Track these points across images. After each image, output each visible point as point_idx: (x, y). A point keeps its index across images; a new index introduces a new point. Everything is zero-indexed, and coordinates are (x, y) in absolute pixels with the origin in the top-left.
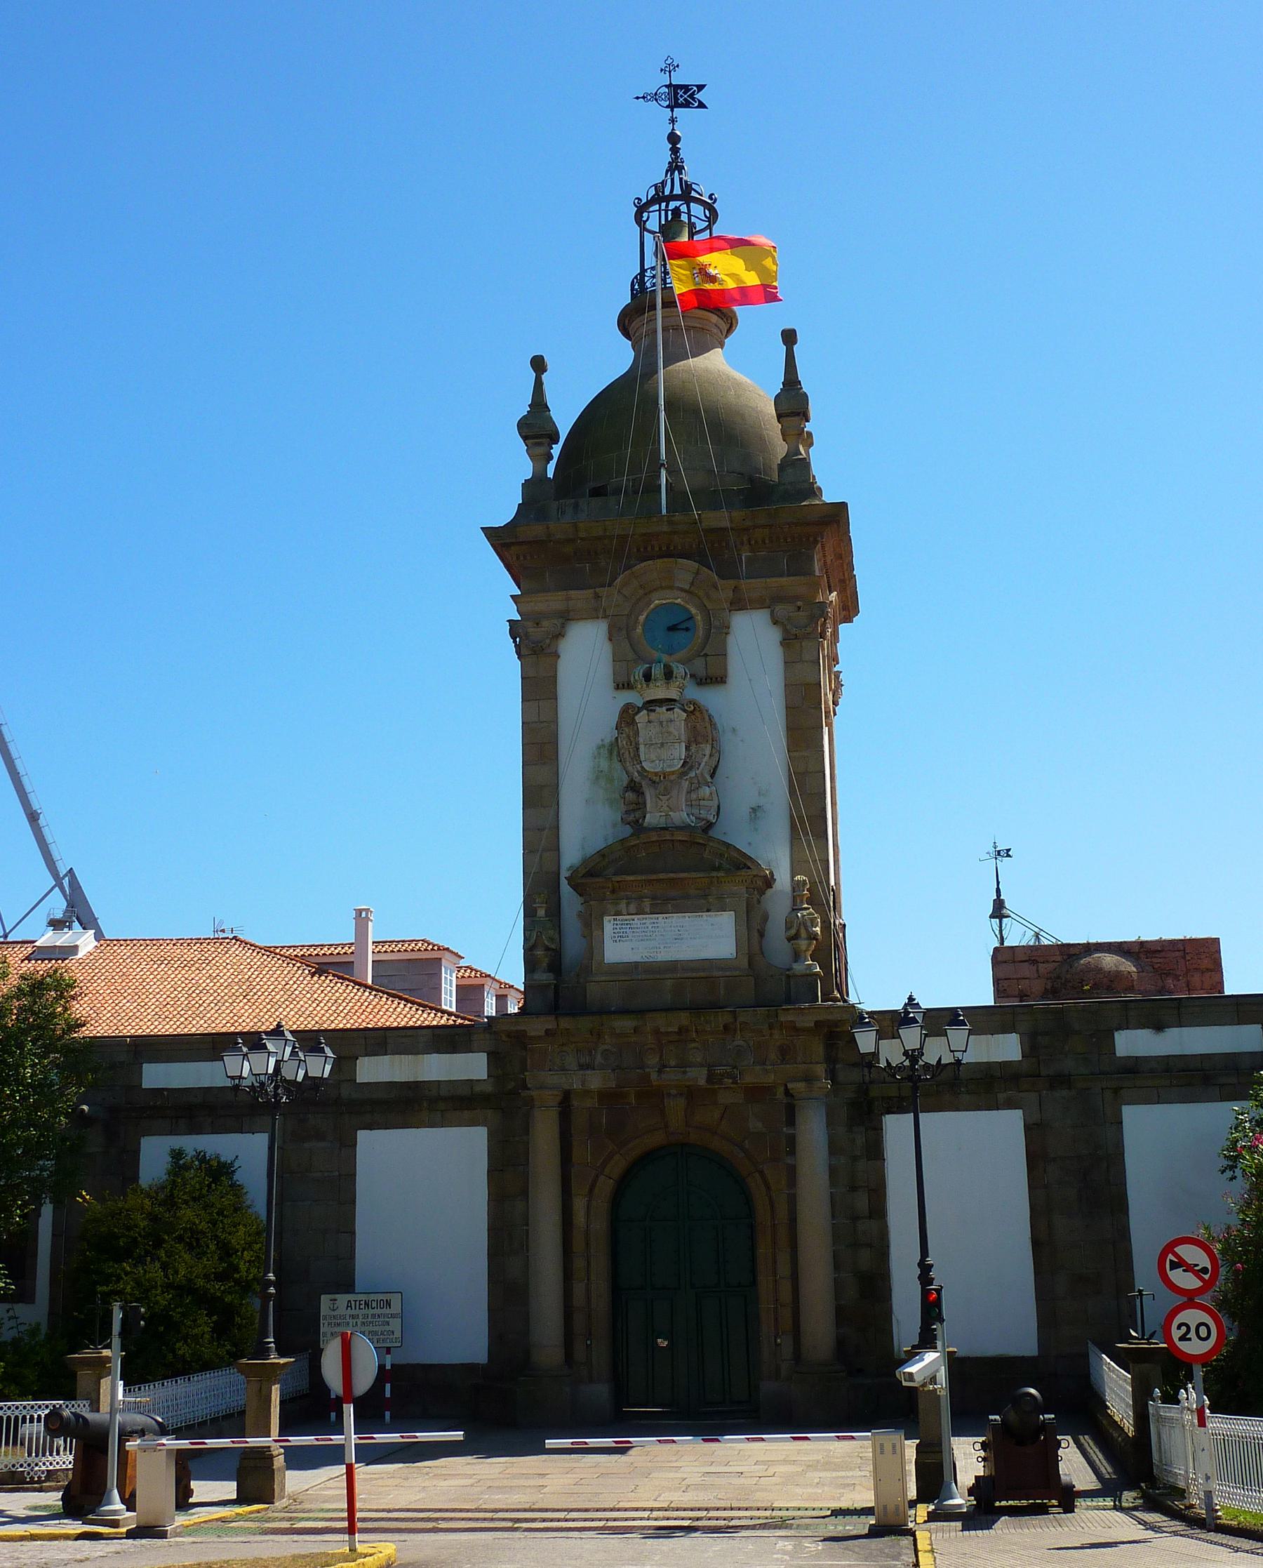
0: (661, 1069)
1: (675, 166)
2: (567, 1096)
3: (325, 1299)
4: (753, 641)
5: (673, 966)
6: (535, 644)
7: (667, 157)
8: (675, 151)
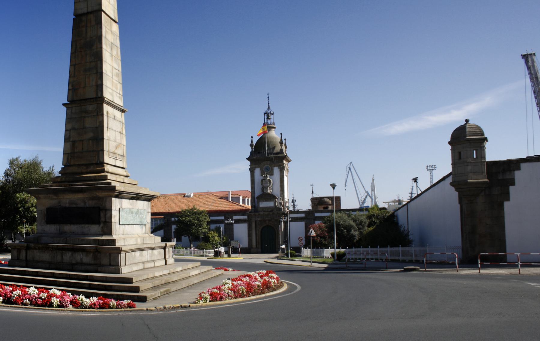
1: (269, 107)
4: (276, 170)
5: (267, 207)
6: (252, 171)
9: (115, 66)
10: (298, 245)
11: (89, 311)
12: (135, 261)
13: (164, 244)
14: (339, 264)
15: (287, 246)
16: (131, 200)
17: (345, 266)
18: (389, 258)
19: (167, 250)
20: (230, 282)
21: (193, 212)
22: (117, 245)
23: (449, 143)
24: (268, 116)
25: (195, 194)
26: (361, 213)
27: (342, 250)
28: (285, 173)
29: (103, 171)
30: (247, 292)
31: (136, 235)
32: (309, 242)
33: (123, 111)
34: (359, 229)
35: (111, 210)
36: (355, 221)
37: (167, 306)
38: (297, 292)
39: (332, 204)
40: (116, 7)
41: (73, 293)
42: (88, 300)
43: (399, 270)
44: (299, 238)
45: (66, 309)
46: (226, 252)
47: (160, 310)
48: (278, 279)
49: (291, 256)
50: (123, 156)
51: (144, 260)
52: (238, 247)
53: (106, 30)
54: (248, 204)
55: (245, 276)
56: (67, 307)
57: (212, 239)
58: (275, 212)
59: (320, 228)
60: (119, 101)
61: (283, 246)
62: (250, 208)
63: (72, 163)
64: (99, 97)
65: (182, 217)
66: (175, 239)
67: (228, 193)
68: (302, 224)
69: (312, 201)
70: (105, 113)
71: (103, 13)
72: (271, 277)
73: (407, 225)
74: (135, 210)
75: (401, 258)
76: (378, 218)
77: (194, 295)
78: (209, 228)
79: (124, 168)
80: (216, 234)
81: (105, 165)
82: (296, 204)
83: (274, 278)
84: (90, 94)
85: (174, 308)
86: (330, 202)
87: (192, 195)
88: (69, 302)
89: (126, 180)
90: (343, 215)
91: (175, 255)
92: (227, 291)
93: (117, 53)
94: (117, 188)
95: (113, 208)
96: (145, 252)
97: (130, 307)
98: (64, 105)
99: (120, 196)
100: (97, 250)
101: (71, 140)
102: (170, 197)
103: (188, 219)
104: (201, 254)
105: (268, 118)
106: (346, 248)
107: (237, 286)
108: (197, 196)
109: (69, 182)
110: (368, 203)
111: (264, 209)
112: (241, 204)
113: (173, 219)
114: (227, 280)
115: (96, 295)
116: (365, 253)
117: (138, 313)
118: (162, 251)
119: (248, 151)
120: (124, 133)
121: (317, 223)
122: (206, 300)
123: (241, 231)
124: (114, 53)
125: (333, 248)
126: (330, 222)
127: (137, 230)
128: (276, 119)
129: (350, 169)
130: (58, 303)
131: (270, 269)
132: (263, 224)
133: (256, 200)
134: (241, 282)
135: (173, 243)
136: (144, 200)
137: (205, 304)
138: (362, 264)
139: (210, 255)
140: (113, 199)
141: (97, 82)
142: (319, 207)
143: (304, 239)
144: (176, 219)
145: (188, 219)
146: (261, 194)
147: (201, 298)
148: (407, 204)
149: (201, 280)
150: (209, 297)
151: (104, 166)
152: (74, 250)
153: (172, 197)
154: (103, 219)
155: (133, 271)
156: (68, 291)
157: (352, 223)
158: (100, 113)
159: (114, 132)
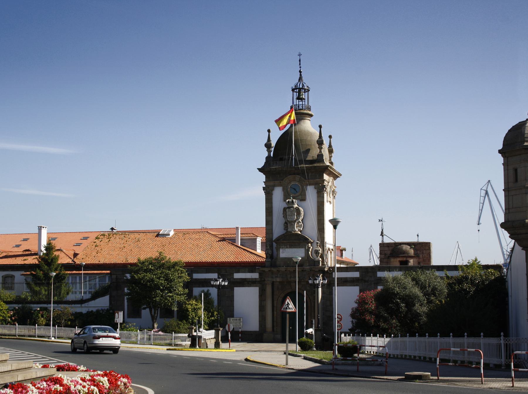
0: (291, 277)
1: (300, 79)
2: (273, 282)
3: (228, 319)
4: (311, 192)
6: (268, 191)
8: (301, 75)
21: (159, 265)
23: (500, 152)
24: (299, 92)
25: (177, 231)
36: (422, 287)
57: (192, 314)
65: (137, 272)
86: (412, 252)
87: (172, 233)
102: (132, 236)
103: (149, 276)
104: (168, 342)
105: (299, 98)
119: (261, 156)
123: (247, 301)
128: (314, 101)
129: (487, 193)
133: (275, 245)
139: (184, 343)
142: (392, 260)
145: (149, 276)
146: (283, 235)
153: (136, 235)
157: (417, 291)
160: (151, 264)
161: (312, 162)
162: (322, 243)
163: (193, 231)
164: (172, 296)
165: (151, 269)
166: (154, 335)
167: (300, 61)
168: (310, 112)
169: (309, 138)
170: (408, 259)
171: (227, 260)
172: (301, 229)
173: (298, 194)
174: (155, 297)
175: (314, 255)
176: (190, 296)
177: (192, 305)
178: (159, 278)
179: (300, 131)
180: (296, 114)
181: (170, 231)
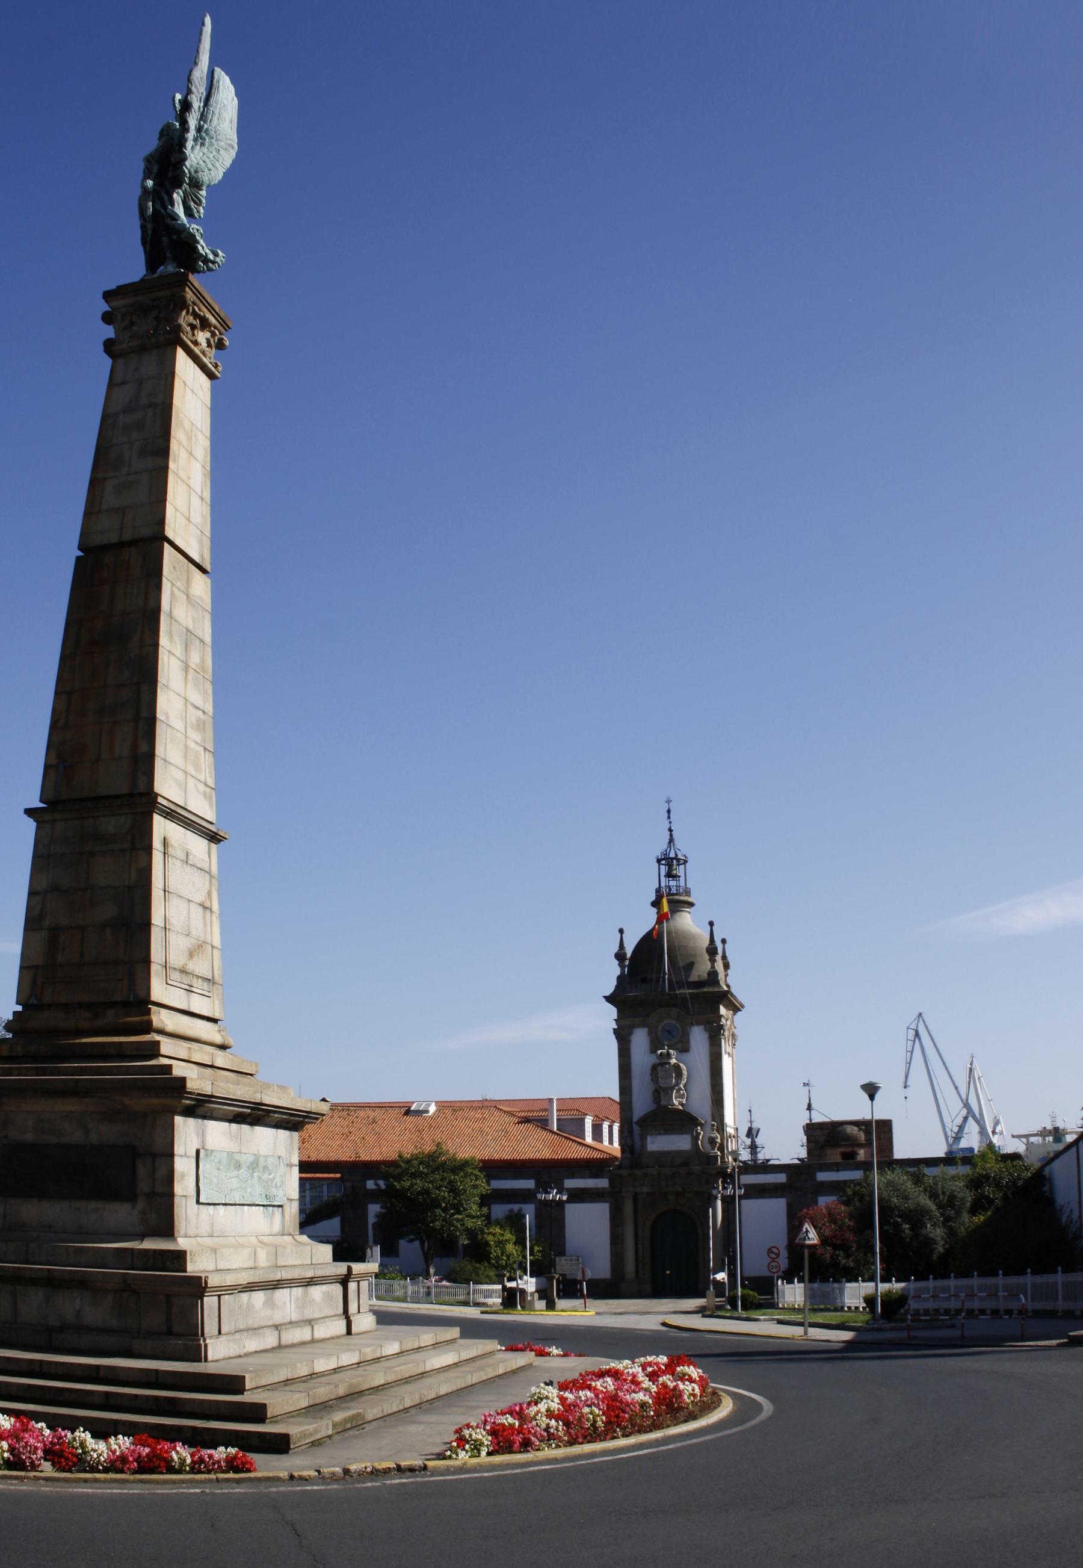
1: (671, 840)
4: (698, 1037)
5: (670, 1153)
6: (622, 1036)
7: (668, 837)
8: (671, 835)
9: (195, 697)
10: (765, 1273)
11: (105, 1481)
12: (251, 1323)
13: (341, 1268)
14: (888, 1331)
15: (732, 1275)
16: (234, 1125)
17: (904, 1334)
18: (1030, 1306)
19: (352, 1286)
20: (553, 1392)
21: (436, 1165)
22: (193, 1267)
24: (670, 866)
25: (442, 1106)
26: (952, 1171)
27: (897, 1286)
28: (726, 1047)
29: (147, 1027)
30: (607, 1423)
31: (254, 1239)
32: (800, 1263)
33: (214, 838)
34: (947, 1219)
35: (171, 1155)
36: (933, 1196)
37: (353, 1467)
38: (763, 1423)
39: (868, 1144)
40: (208, 532)
41: (53, 1422)
42: (101, 1446)
43: (1054, 1342)
44: (770, 1251)
45: (32, 1474)
46: (543, 1293)
47: (334, 1478)
48: (703, 1383)
49: (744, 1308)
50: (211, 981)
51: (278, 1318)
52: (580, 1277)
53: (172, 593)
54: (611, 1141)
55: (601, 1374)
56: (34, 1467)
57: (495, 1252)
58: (696, 1168)
59: (832, 1217)
60: (203, 808)
61: (721, 1276)
62: (618, 1154)
63: (47, 999)
64: (141, 794)
65: (399, 1178)
66: (377, 1250)
67: (546, 1106)
68: (777, 1207)
69: (806, 1133)
70: (157, 843)
71: (166, 545)
72: (683, 1378)
73: (1077, 1205)
74: (246, 1159)
75: (1061, 1305)
76: (998, 1185)
77: (436, 1431)
78: (488, 1217)
79: (215, 1021)
80: (508, 1236)
81: (154, 1008)
82: (759, 1141)
83: (691, 1380)
84: (113, 781)
85: (375, 1473)
86: (862, 1136)
88: (40, 1453)
89: (221, 1059)
90: (898, 1176)
91: (378, 1298)
92: (544, 1421)
93: (203, 661)
94: (191, 1085)
95: (178, 1149)
96: (282, 1295)
97: (237, 1470)
98: (29, 812)
99: (199, 1111)
100: (126, 1286)
101: (46, 923)
102: (362, 1113)
103: (419, 1184)
104: (462, 1298)
105: (670, 875)
106: (907, 1280)
107: (575, 1405)
108: (448, 1112)
109: (34, 1058)
110: (971, 1140)
111: (662, 1157)
112: (589, 1139)
113: (370, 1185)
114: (544, 1386)
115: (129, 1429)
116: (962, 1295)
117: (262, 1489)
118: (338, 1289)
119: (609, 975)
120: (216, 907)
121: (824, 1201)
122: (477, 1447)
123: (588, 1227)
124: (195, 659)
125: (872, 1279)
126: (862, 1199)
127: (257, 1221)
128: (694, 878)
129: (917, 1034)
130: (6, 1455)
131: (681, 1348)
132: (654, 1202)
133: (636, 1128)
134: (589, 1394)
135: (373, 1266)
136: (278, 1126)
137: (475, 1460)
138: (952, 1326)
139: (490, 1301)
140: (179, 1120)
141: (135, 746)
142: (828, 1151)
143: (784, 1253)
144: (381, 1183)
146: (656, 1110)
147: (462, 1441)
148: (1075, 1143)
149: (460, 1384)
150: (487, 1440)
151: (148, 1012)
152: (52, 1283)
154: (143, 1186)
155: (247, 1355)
156: (38, 1417)
157: (925, 1201)
158: (140, 844)
159: (183, 905)
160: (421, 1163)
161: (700, 984)
162: (721, 1126)
163: (469, 1105)
164: (462, 1220)
165: (422, 1173)
166: (436, 1287)
167: (669, 811)
168: (690, 900)
169: (691, 944)
170: (856, 1149)
171: (538, 1156)
172: (684, 1101)
173: (675, 1040)
174: (432, 1222)
175: (708, 1146)
176: (488, 1220)
177: (494, 1235)
178: (438, 1188)
179: (677, 932)
180: (669, 902)
181: (429, 1105)
